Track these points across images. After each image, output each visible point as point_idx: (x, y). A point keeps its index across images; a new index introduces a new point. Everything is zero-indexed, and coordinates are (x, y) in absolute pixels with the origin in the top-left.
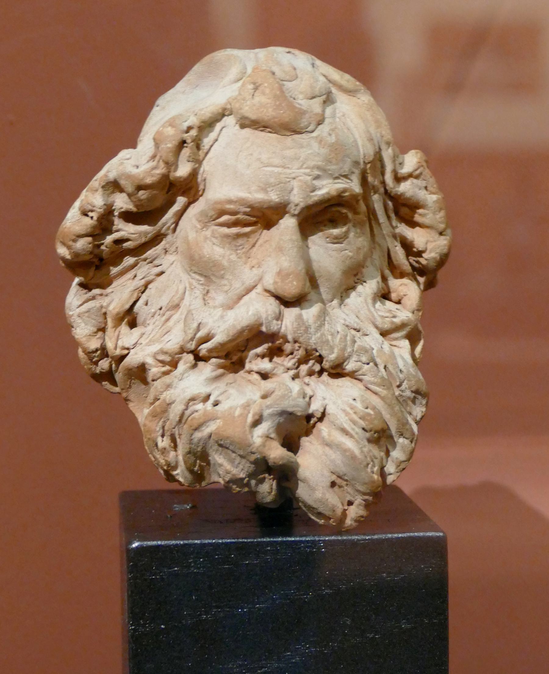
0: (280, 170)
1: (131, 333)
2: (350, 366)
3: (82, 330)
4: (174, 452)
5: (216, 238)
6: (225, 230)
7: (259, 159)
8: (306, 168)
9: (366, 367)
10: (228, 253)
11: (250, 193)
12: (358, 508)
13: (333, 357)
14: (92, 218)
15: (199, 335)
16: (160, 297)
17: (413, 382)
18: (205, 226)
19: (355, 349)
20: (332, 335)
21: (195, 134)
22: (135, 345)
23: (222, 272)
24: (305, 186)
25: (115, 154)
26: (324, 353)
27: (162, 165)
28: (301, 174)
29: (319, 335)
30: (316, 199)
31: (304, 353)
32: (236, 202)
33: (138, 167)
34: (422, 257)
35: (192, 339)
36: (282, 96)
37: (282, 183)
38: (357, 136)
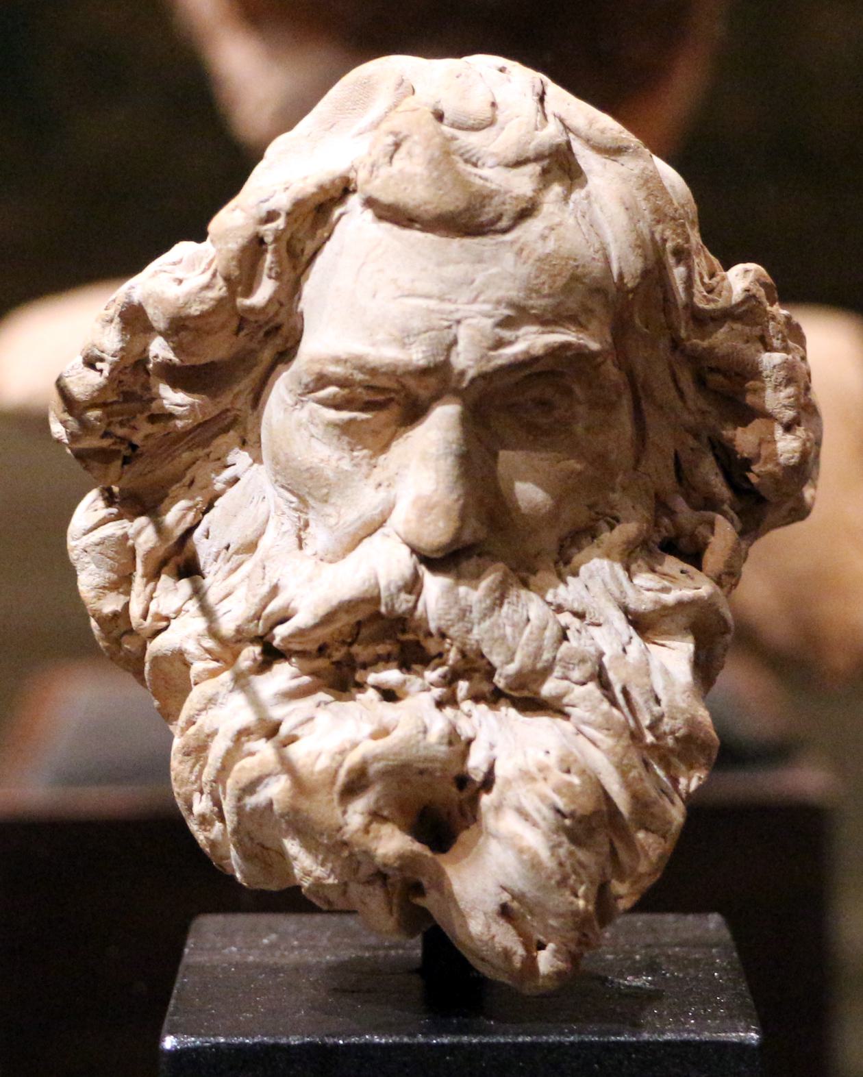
0: (433, 304)
1: (176, 589)
2: (549, 688)
3: (89, 579)
4: (221, 824)
5: (317, 426)
6: (332, 415)
7: (394, 281)
8: (484, 302)
9: (579, 690)
10: (336, 455)
11: (373, 345)
12: (555, 956)
13: (512, 668)
14: (101, 371)
15: (273, 606)
16: (227, 526)
17: (678, 721)
18: (299, 402)
19: (559, 656)
20: (514, 625)
21: (282, 227)
22: (178, 612)
23: (325, 491)
24: (479, 338)
25: (167, 247)
26: (496, 660)
27: (220, 282)
28: (472, 314)
29: (487, 624)
30: (500, 362)
31: (459, 657)
32: (346, 361)
33: (180, 281)
34: (751, 471)
35: (257, 617)
36: (447, 157)
37: (433, 329)
38: (609, 237)
